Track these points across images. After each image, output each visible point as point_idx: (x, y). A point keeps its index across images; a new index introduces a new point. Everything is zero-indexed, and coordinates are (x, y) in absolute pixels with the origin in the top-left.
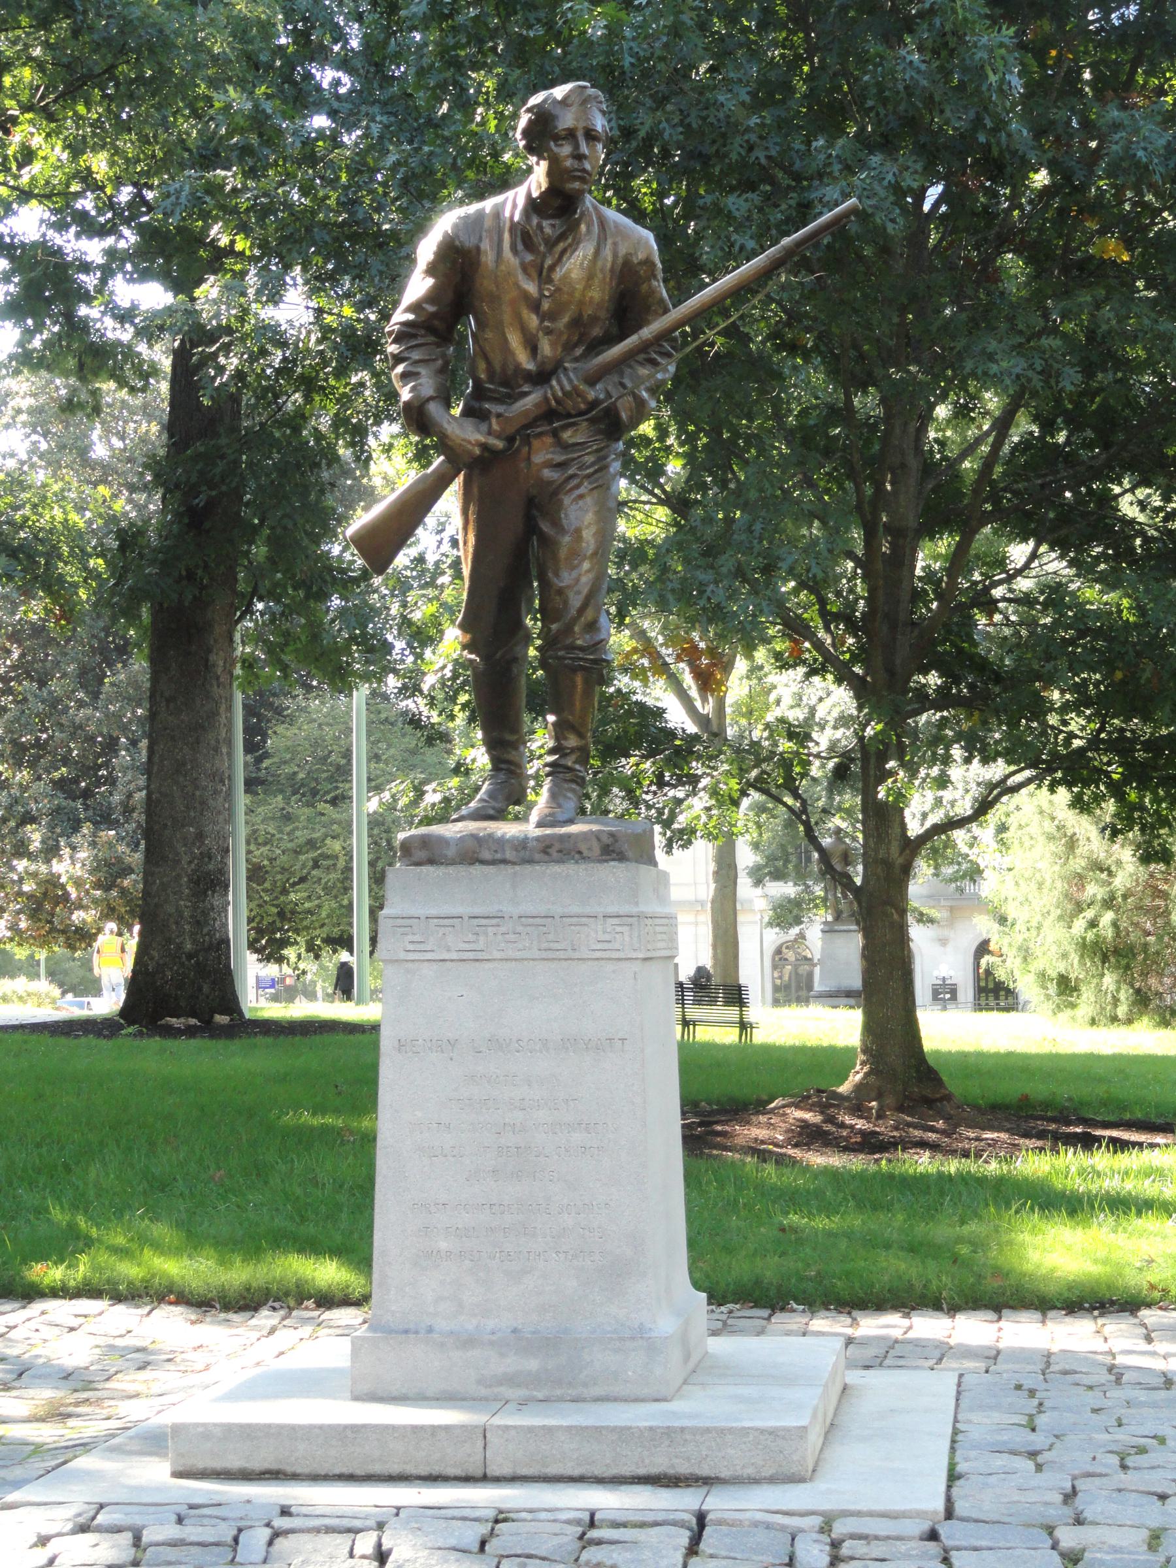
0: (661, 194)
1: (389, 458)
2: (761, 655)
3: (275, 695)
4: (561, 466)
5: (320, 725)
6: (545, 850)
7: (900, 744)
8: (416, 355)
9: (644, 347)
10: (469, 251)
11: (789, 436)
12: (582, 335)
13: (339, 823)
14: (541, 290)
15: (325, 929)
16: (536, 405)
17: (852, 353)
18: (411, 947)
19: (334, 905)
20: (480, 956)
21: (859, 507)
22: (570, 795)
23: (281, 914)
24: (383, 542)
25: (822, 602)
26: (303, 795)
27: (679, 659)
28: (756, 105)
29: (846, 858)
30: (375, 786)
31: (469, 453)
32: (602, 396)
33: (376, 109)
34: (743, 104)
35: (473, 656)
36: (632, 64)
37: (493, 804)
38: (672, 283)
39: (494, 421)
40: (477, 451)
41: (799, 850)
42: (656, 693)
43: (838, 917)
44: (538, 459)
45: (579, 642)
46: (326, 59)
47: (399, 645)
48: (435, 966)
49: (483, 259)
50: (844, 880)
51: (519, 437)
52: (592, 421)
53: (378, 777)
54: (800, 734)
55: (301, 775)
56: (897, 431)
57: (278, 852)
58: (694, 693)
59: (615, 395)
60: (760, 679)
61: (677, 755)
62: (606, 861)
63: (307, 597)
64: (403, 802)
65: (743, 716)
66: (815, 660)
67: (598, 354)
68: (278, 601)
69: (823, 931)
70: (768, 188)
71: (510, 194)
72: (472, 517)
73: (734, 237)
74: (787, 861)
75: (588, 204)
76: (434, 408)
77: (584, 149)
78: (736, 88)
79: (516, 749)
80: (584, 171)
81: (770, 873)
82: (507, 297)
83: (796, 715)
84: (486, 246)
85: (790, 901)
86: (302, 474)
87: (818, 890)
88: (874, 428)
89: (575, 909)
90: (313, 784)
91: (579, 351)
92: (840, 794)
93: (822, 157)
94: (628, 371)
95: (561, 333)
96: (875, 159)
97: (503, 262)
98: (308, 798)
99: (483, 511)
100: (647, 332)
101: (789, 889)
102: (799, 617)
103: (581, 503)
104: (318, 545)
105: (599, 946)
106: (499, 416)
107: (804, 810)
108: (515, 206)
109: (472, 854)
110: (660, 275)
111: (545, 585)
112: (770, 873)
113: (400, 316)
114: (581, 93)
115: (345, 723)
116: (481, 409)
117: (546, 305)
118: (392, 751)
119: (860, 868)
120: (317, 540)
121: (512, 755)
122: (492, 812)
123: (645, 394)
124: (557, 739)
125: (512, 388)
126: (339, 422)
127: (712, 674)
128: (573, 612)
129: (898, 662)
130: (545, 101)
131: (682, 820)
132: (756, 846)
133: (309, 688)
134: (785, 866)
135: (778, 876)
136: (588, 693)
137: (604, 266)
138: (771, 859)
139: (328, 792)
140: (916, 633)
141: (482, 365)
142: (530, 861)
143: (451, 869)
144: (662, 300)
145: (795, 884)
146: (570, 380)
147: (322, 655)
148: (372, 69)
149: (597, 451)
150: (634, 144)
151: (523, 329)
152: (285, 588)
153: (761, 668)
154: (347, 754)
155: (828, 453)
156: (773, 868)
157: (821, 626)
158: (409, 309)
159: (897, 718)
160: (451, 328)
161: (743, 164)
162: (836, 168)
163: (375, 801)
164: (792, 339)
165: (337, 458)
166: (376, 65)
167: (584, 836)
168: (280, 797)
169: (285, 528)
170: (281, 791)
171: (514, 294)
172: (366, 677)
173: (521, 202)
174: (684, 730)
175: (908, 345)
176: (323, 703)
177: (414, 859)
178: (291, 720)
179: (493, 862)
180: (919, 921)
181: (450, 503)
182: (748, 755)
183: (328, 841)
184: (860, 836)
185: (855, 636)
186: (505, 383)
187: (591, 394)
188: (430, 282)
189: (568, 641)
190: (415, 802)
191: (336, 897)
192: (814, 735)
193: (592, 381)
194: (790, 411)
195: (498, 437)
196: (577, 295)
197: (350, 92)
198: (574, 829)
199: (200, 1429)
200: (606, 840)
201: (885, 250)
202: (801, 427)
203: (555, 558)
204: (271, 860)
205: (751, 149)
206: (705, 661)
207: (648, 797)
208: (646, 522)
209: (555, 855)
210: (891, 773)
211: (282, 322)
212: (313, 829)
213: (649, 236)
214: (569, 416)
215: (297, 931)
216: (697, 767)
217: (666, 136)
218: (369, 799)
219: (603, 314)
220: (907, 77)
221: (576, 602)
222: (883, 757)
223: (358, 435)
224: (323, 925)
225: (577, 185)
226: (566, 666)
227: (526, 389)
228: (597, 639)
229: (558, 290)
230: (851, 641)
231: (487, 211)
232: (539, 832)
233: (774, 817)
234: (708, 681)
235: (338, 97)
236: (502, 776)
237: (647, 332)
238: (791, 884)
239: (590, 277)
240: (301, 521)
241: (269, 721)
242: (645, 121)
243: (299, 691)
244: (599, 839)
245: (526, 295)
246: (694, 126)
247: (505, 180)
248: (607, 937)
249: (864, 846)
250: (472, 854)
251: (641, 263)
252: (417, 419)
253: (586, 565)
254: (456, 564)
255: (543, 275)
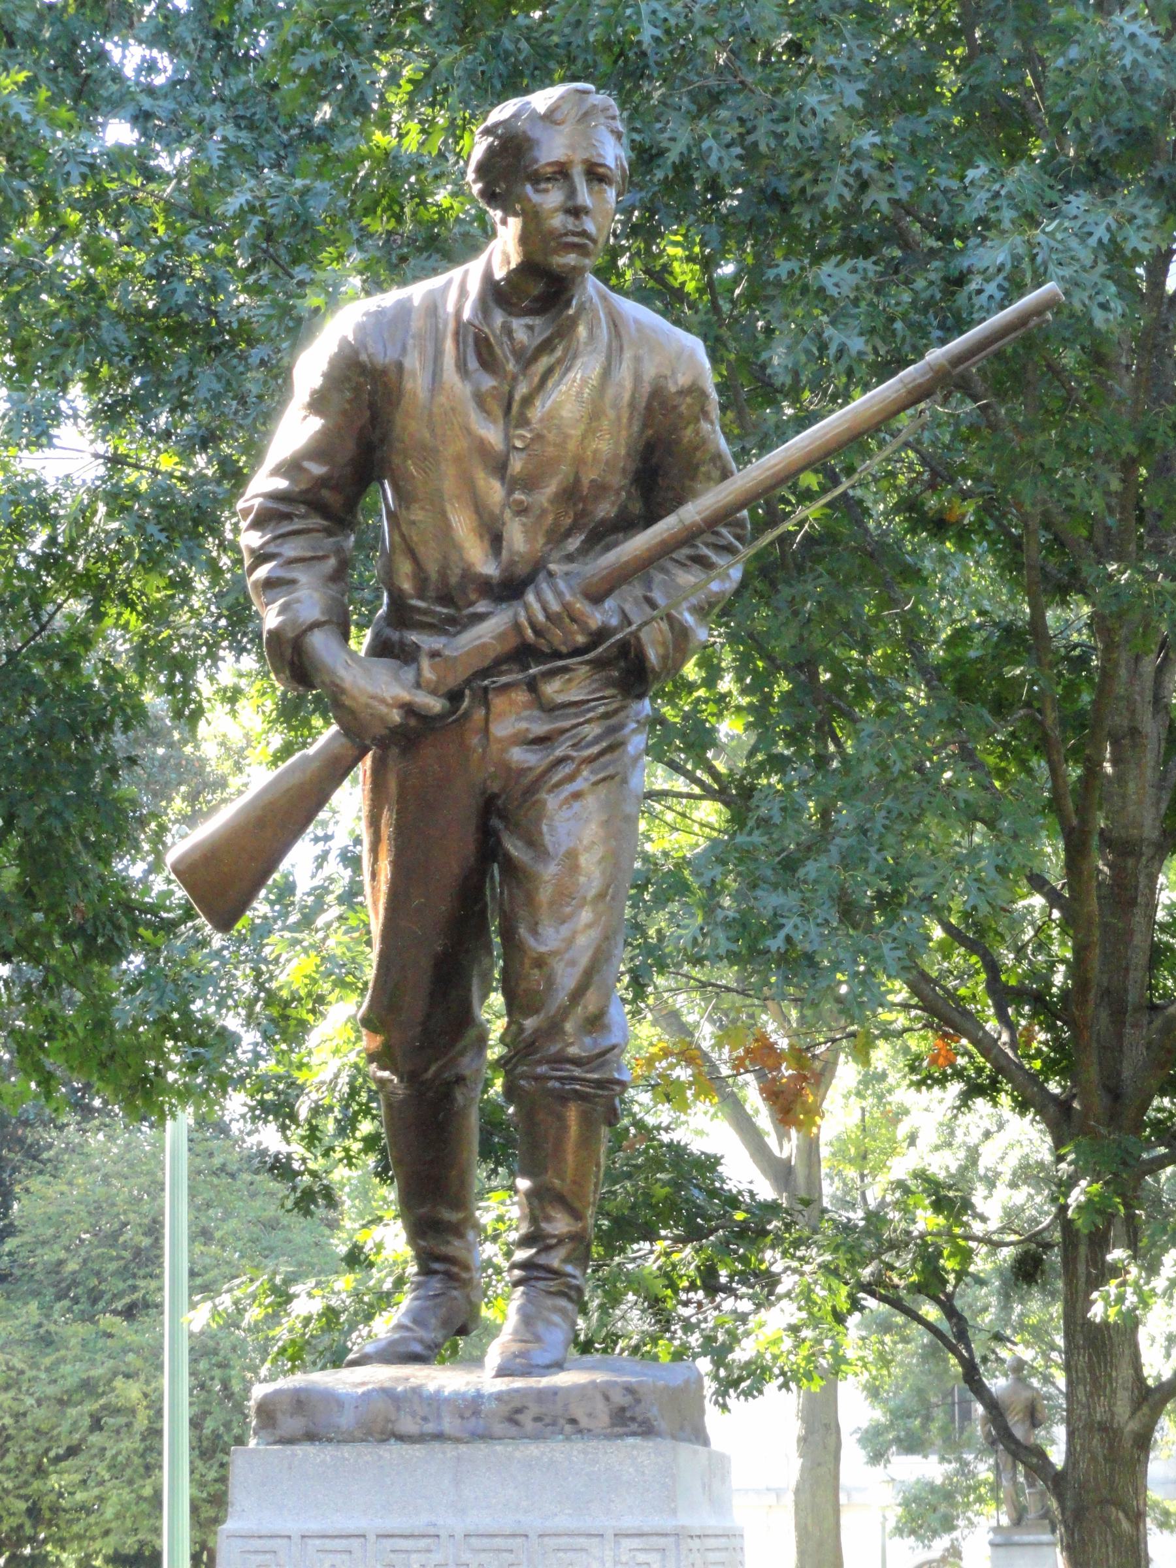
0: (708, 264)
1: (233, 712)
2: (882, 1054)
3: (26, 1123)
4: (542, 741)
5: (106, 1178)
6: (513, 1418)
7: (1131, 1218)
8: (290, 550)
9: (689, 537)
10: (384, 372)
11: (931, 675)
12: (580, 516)
13: (137, 1351)
14: (507, 438)
15: (112, 1540)
16: (501, 637)
17: (1043, 537)
19: (127, 1495)
21: (1055, 805)
22: (556, 1318)
23: (33, 1512)
24: (231, 879)
25: (993, 968)
26: (76, 1300)
27: (738, 1065)
28: (874, 110)
29: (1034, 1417)
30: (203, 1285)
31: (382, 719)
32: (614, 622)
33: (217, 111)
34: (851, 111)
35: (386, 1074)
36: (657, 40)
37: (421, 1333)
38: (730, 415)
39: (425, 663)
40: (396, 716)
41: (954, 1394)
42: (703, 1130)
43: (1019, 1520)
44: (502, 729)
45: (573, 1051)
46: (131, 26)
47: (250, 1038)
49: (408, 385)
50: (1029, 1456)
51: (471, 690)
52: (599, 664)
53: (206, 1269)
54: (950, 1200)
55: (72, 1266)
56: (1123, 672)
57: (30, 1401)
58: (764, 1120)
59: (637, 620)
60: (880, 1097)
61: (733, 1237)
62: (619, 1436)
63: (87, 956)
64: (254, 1314)
65: (851, 1161)
66: (980, 1070)
67: (608, 548)
68: (36, 959)
69: (993, 1545)
70: (898, 253)
71: (456, 273)
72: (386, 831)
73: (830, 331)
74: (928, 1418)
75: (591, 290)
76: (321, 643)
77: (584, 196)
78: (840, 83)
79: (461, 1235)
80: (584, 234)
81: (898, 1441)
82: (450, 451)
83: (943, 1164)
84: (413, 362)
85: (933, 1489)
86: (79, 742)
87: (984, 1470)
88: (1082, 661)
89: (563, 1522)
90: (94, 1282)
91: (574, 544)
92: (1022, 1300)
93: (983, 195)
94: (659, 577)
95: (544, 512)
96: (1078, 202)
97: (443, 396)
98: (83, 1305)
99: (409, 820)
100: (692, 512)
101: (930, 1469)
102: (951, 995)
103: (577, 806)
104: (107, 864)
106: (435, 654)
107: (962, 1335)
108: (463, 293)
109: (387, 1425)
110: (715, 413)
111: (508, 934)
112: (898, 1441)
113: (264, 482)
114: (582, 101)
115: (150, 1173)
116: (402, 644)
117: (517, 465)
118: (233, 1224)
119: (1060, 1432)
120: (103, 854)
121: (455, 1248)
122: (418, 1348)
123: (689, 619)
124: (534, 1219)
125: (458, 609)
126: (147, 654)
127: (799, 1093)
128: (562, 997)
129: (1126, 1074)
130: (516, 116)
131: (741, 1354)
132: (873, 1392)
133: (87, 1111)
134: (924, 1427)
135: (913, 1445)
136: (588, 1140)
137: (618, 397)
138: (899, 1415)
139: (116, 1297)
140: (1158, 1022)
141: (405, 567)
142: (485, 1436)
143: (347, 1451)
144: (718, 457)
145: (943, 1459)
146: (559, 595)
147: (112, 1057)
148: (211, 44)
149: (606, 716)
150: (659, 175)
151: (479, 507)
152: (48, 937)
153: (883, 1076)
154: (154, 1229)
155: (1000, 707)
156: (903, 1434)
157: (991, 1011)
158: (277, 472)
159: (1125, 1176)
160: (351, 504)
161: (851, 212)
162: (1008, 215)
163: (205, 1309)
164: (941, 511)
165: (141, 712)
166: (217, 36)
167: (580, 1391)
168: (33, 1305)
169: (49, 835)
170: (37, 1294)
171: (461, 445)
172: (186, 1094)
173: (474, 288)
174: (752, 1195)
175: (1140, 520)
176: (110, 1138)
177: (279, 1433)
178: (55, 1169)
179: (420, 1438)
180: (1163, 1525)
181: (350, 802)
182: (862, 1245)
183: (119, 1382)
184: (1061, 1379)
185: (1051, 1028)
186: (446, 598)
187: (596, 618)
188: (316, 423)
189: (554, 1049)
190: (273, 1318)
191: (131, 1482)
192: (977, 1199)
193: (596, 598)
194: (933, 632)
195: (433, 692)
196: (572, 446)
197: (174, 83)
198: (563, 1379)
200: (619, 1399)
201: (1097, 358)
202: (954, 664)
203: (530, 900)
204: (18, 1416)
205: (864, 186)
206: (787, 1071)
207: (685, 1312)
208: (682, 826)
209: (529, 1426)
210: (1116, 1271)
211: (51, 481)
212: (92, 1361)
213: (695, 345)
214: (557, 655)
215: (62, 1543)
216: (772, 1259)
217: (713, 162)
218: (193, 1306)
219: (617, 480)
220: (1127, 61)
221: (567, 979)
222: (1100, 1242)
223: (179, 669)
224: (107, 1533)
225: (571, 259)
226: (551, 1092)
227: (481, 607)
228: (605, 1043)
229: (539, 437)
230: (1042, 1036)
231: (416, 302)
232: (502, 1384)
233: (906, 1340)
234: (790, 1105)
235: (150, 91)
236: (436, 1284)
237: (692, 512)
238: (934, 1458)
239: (595, 415)
240: (76, 822)
241: (15, 1169)
242: (677, 137)
243: (70, 1118)
244: (607, 1398)
245: (482, 449)
246: (763, 148)
247: (438, 246)
249: (1070, 1395)
250: (387, 1425)
251: (682, 393)
252: (292, 660)
253: (586, 915)
254: (351, 896)
255: (512, 411)
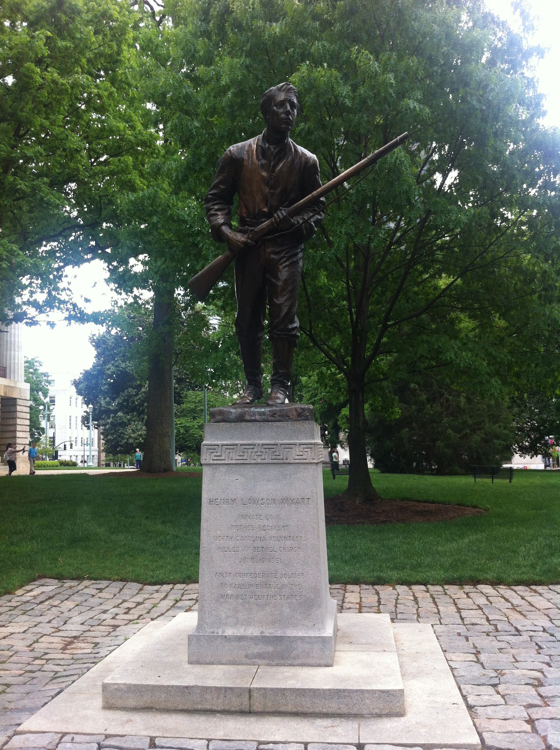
18: (215, 458)
20: (246, 462)
40: (242, 246)
48: (226, 467)
51: (261, 240)
62: (299, 420)
105: (298, 457)
199: (116, 687)
200: (299, 411)
236: (252, 387)
248: (301, 453)
